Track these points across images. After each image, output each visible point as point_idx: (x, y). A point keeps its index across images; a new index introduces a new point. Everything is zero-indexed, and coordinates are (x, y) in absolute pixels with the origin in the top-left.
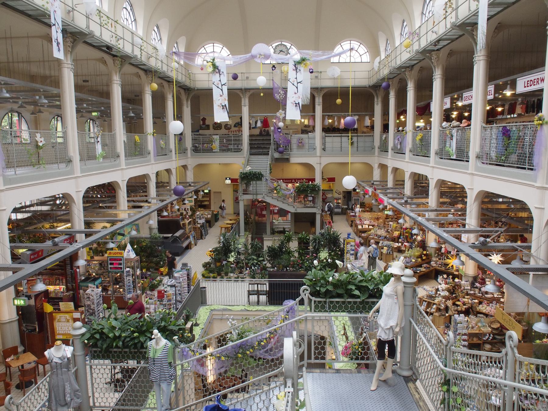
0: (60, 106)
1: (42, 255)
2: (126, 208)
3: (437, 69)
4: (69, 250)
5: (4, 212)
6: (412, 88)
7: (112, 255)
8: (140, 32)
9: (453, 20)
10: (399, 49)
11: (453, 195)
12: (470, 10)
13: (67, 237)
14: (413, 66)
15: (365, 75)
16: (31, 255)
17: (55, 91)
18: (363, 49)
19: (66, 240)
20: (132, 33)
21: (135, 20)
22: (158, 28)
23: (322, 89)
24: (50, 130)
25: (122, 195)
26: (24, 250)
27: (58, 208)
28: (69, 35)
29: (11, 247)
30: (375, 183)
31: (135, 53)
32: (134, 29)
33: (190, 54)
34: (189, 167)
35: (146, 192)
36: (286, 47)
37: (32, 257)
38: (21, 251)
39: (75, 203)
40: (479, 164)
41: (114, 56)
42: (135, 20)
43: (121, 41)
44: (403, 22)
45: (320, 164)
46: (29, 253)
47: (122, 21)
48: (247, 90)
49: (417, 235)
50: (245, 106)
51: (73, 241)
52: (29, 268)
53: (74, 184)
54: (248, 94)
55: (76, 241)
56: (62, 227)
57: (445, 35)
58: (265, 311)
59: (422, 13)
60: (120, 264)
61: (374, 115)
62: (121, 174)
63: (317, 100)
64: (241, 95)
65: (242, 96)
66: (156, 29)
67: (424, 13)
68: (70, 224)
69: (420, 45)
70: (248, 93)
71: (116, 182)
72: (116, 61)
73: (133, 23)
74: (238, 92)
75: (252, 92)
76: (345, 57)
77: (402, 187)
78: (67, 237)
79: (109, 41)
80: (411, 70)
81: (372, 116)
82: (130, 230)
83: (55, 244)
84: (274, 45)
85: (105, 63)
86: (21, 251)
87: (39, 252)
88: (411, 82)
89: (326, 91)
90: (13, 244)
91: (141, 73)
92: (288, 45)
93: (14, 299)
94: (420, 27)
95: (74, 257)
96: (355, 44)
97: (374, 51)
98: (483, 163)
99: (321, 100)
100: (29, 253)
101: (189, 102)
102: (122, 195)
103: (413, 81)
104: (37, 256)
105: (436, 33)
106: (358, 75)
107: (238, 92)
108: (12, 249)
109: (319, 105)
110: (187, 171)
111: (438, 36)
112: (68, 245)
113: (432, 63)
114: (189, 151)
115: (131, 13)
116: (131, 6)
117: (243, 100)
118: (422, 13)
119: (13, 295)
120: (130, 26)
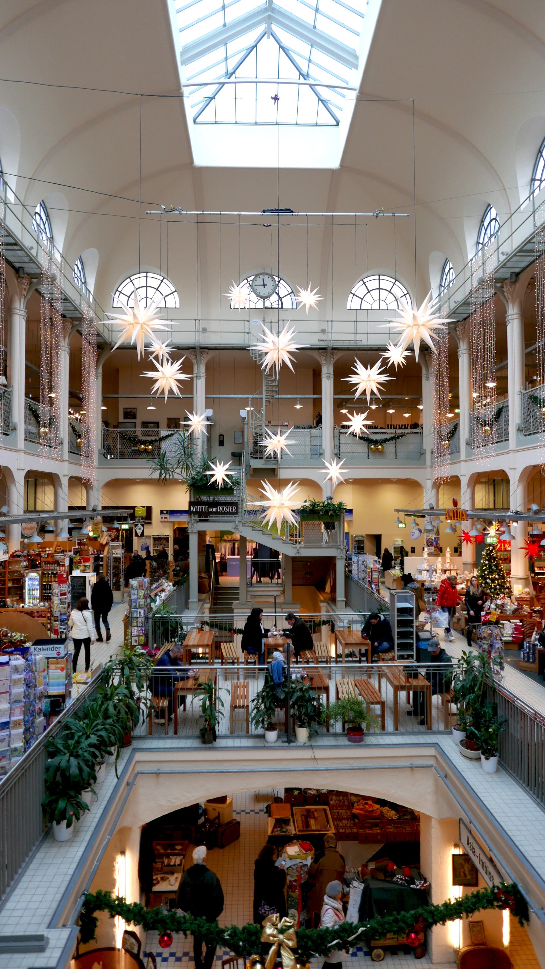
3: (461, 343)
11: (496, 481)
24: (39, 402)
28: (26, 275)
34: (95, 484)
39: (61, 487)
40: (522, 437)
49: (463, 664)
54: (205, 358)
58: (385, 433)
65: (194, 361)
70: (205, 355)
75: (338, 355)
76: (371, 301)
88: (463, 342)
98: (525, 435)
101: (100, 370)
107: (315, 354)
110: (91, 492)
114: (96, 456)
115: (47, 225)
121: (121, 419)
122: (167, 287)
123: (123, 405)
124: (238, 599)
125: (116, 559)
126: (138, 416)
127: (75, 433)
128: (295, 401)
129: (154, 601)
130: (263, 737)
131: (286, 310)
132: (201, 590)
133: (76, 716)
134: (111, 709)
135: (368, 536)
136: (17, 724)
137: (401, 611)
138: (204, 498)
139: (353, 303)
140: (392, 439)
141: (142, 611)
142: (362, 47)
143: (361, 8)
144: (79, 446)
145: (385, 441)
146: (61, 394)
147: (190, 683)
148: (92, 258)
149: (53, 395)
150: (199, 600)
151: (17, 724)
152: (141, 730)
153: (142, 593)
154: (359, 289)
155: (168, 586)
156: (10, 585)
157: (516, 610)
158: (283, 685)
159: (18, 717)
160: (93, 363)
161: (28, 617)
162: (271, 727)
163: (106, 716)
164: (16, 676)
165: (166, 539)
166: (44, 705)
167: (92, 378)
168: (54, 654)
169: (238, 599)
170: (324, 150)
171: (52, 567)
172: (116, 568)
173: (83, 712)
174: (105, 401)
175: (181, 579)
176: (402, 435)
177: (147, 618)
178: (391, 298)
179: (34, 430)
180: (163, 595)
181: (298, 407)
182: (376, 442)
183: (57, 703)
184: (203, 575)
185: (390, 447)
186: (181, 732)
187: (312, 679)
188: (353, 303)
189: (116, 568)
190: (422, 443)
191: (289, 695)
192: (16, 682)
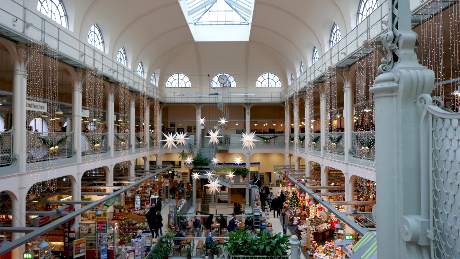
0: (71, 113)
1: (48, 220)
2: (113, 185)
3: (346, 82)
4: (69, 216)
5: (24, 189)
6: (348, 89)
7: (99, 220)
8: (129, 67)
9: (309, 80)
10: (298, 80)
12: (339, 60)
13: (68, 206)
14: (350, 66)
15: (279, 95)
16: (40, 220)
17: (69, 105)
18: (276, 79)
19: (66, 209)
20: (124, 68)
21: (143, 71)
22: (141, 64)
23: (250, 104)
25: (110, 176)
26: (36, 216)
27: (64, 185)
29: (26, 214)
30: (286, 167)
31: (96, 66)
32: (125, 65)
33: (163, 80)
35: (105, 180)
36: (227, 77)
37: (41, 221)
38: (33, 217)
39: (16, 199)
41: (111, 83)
42: (143, 71)
43: (116, 73)
44: (314, 49)
45: (249, 154)
46: (40, 218)
47: (117, 60)
48: (200, 104)
50: (198, 114)
51: (72, 209)
52: (38, 231)
53: (76, 169)
54: (200, 107)
55: (74, 210)
56: (65, 199)
57: (342, 63)
59: (313, 58)
60: (104, 227)
61: (285, 121)
62: (109, 162)
63: (247, 111)
64: (195, 106)
66: (140, 64)
67: (332, 40)
68: (71, 197)
69: (310, 79)
71: (107, 167)
72: (20, 49)
73: (101, 44)
74: (194, 105)
75: (203, 105)
76: (265, 83)
77: (304, 170)
78: (68, 206)
79: (10, 26)
80: (349, 70)
81: (283, 122)
82: (114, 201)
83: (59, 212)
84: (218, 75)
85: (68, 73)
86: (33, 217)
87: (46, 217)
89: (252, 105)
90: (28, 212)
91: (71, 70)
92: (228, 75)
93: (24, 254)
94: (310, 67)
95: (71, 221)
96: (271, 76)
97: (284, 80)
99: (249, 111)
100: (40, 218)
101: (161, 111)
102: (110, 176)
103: (350, 81)
104: (44, 221)
105: (344, 54)
106: (274, 95)
108: (82, 194)
109: (248, 114)
111: (346, 56)
112: (67, 213)
113: (343, 77)
115: (124, 55)
116: (124, 51)
117: (197, 110)
118: (313, 58)
119: (24, 251)
120: (123, 64)
121: (169, 127)
122: (186, 79)
123: (170, 121)
124: (211, 202)
125: (167, 187)
126: (176, 125)
127: (152, 138)
128: (236, 122)
129: (178, 209)
130: (204, 257)
131: (232, 87)
132: (198, 196)
133: (153, 252)
134: (162, 250)
135: (266, 173)
136: (140, 255)
137: (256, 216)
138: (198, 167)
139: (258, 84)
140: (273, 138)
141: (173, 214)
142: (252, 9)
143: (251, 2)
144: (153, 143)
145: (270, 138)
146: (146, 124)
147: (185, 242)
148: (158, 71)
149: (144, 124)
150: (196, 202)
151: (140, 255)
152: (171, 255)
153: (173, 208)
154: (260, 79)
155: (184, 201)
156: (130, 200)
157: (300, 214)
158: (210, 243)
159: (140, 254)
160: (158, 112)
161: (137, 216)
162: (207, 255)
163: (161, 252)
164: (139, 244)
165: (187, 174)
166: (145, 249)
167: (158, 114)
168: (147, 236)
169: (211, 202)
170: (242, 34)
171: (144, 194)
172: (167, 190)
173: (155, 251)
174: (163, 122)
175: (189, 198)
176: (277, 136)
177: (175, 216)
178: (273, 82)
179: (137, 143)
180: (182, 206)
181: (237, 124)
182: (266, 139)
183: (148, 249)
184: (200, 190)
185: (272, 141)
186: (182, 255)
187: (219, 241)
188: (258, 84)
189: (167, 190)
190: (285, 139)
191: (211, 246)
192: (139, 246)
